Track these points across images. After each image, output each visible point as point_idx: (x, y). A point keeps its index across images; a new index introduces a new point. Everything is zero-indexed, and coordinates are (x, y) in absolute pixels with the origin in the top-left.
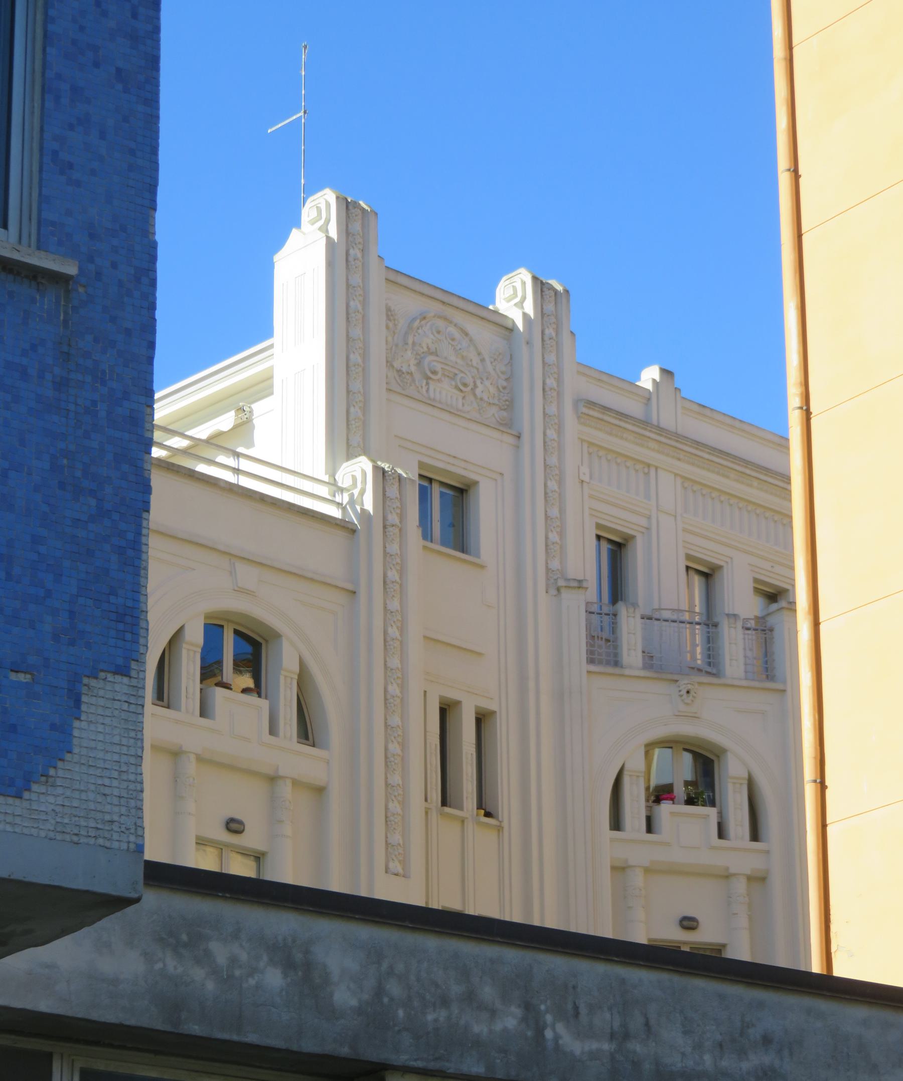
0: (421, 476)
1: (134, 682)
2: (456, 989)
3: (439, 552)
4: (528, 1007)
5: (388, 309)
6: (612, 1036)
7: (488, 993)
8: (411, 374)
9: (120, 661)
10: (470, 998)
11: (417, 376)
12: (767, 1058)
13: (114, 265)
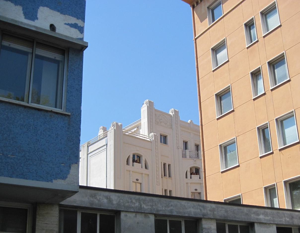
1: (78, 165)
2: (130, 201)
4: (139, 203)
5: (155, 114)
6: (151, 206)
7: (134, 201)
9: (76, 162)
10: (132, 202)
11: (160, 122)
12: (172, 208)
13: (76, 113)
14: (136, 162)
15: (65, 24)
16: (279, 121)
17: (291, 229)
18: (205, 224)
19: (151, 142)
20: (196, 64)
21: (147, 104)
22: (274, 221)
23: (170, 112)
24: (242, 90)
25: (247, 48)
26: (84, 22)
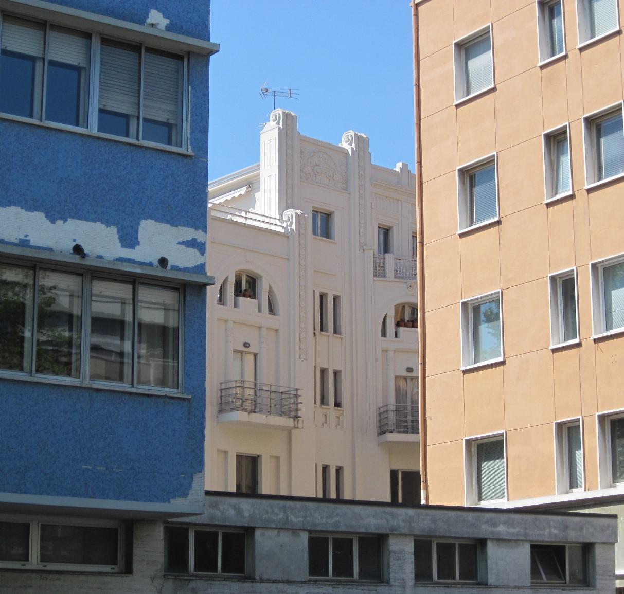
0: (313, 211)
3: (320, 239)
4: (285, 512)
5: (301, 151)
6: (303, 517)
7: (276, 510)
8: (309, 174)
10: (273, 511)
12: (338, 519)
14: (244, 296)
15: (179, 243)
16: (599, 269)
17: (564, 547)
18: (394, 544)
19: (288, 237)
20: (415, 76)
21: (278, 123)
22: (526, 535)
23: (344, 139)
24: (521, 176)
25: (542, 67)
26: (206, 232)
